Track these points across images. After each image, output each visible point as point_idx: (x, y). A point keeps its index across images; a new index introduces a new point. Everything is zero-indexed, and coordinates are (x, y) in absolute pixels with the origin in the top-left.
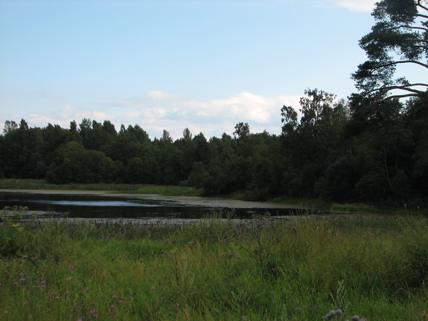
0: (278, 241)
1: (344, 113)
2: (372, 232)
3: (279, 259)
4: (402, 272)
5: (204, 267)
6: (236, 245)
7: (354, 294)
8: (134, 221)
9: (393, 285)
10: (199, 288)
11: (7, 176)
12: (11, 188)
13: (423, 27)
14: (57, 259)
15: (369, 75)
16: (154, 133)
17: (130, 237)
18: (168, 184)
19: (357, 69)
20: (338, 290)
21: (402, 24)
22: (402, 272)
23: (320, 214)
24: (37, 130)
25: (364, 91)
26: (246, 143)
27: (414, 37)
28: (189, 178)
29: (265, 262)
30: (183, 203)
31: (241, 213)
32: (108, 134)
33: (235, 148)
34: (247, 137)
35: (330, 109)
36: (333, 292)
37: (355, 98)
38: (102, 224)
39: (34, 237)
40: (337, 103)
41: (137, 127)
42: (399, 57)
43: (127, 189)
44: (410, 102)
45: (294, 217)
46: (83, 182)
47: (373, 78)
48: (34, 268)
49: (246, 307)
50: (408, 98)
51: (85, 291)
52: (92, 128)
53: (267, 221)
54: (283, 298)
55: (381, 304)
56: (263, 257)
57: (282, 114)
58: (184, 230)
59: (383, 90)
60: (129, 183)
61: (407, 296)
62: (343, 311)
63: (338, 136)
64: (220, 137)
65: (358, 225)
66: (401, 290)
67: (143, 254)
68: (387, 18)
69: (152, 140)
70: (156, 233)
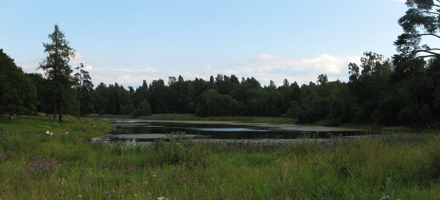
0: (348, 153)
1: (390, 68)
2: (408, 145)
3: (348, 165)
4: (427, 169)
5: (299, 171)
6: (320, 156)
7: (397, 185)
8: (252, 141)
9: (422, 178)
10: (295, 185)
11: (171, 112)
12: (173, 120)
13: (437, 12)
14: (204, 166)
15: (405, 43)
16: (264, 83)
17: (249, 152)
18: (274, 116)
19: (397, 39)
20: (387, 183)
21: (424, 10)
22: (427, 169)
23: (375, 134)
24: (189, 81)
25: (402, 53)
26: (325, 87)
27: (432, 19)
28: (288, 112)
29: (339, 167)
30: (284, 129)
31: (323, 135)
32: (234, 84)
33: (318, 91)
34: (326, 84)
35: (380, 65)
36: (384, 185)
37: (396, 58)
38: (231, 143)
39: (190, 151)
40: (385, 61)
41: (253, 78)
42: (423, 31)
43: (247, 120)
44: (431, 61)
45: (358, 137)
46: (218, 115)
47: (407, 44)
48: (191, 171)
49: (327, 197)
50: (429, 58)
51: (221, 187)
52: (224, 80)
53: (340, 139)
54: (352, 190)
55: (414, 191)
56: (338, 164)
57: (349, 68)
58: (285, 146)
59: (414, 53)
60: (248, 116)
61: (430, 185)
62: (390, 197)
63: (386, 82)
64: (308, 84)
65: (399, 140)
66: (427, 181)
67: (258, 163)
68: (415, 6)
69: (263, 87)
70: (267, 149)
